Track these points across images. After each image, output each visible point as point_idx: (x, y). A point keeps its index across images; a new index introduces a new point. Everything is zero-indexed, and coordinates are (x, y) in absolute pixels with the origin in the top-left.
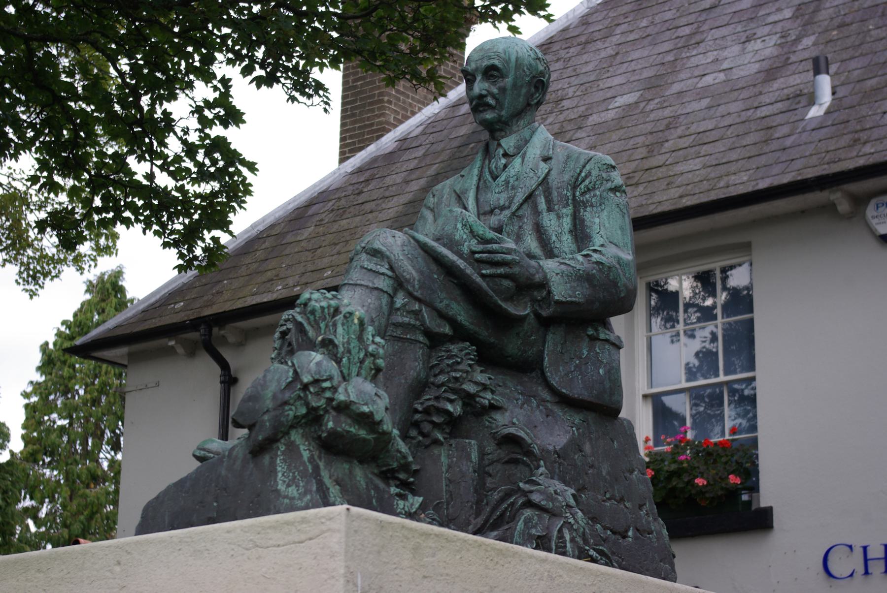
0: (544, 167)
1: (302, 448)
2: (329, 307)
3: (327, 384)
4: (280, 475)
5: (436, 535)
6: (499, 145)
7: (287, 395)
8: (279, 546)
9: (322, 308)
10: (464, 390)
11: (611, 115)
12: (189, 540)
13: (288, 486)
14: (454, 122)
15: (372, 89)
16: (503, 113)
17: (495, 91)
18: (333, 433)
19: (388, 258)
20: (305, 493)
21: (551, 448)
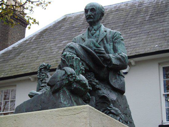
0: (105, 33)
1: (67, 92)
2: (72, 56)
3: (74, 75)
4: (61, 98)
5: (105, 116)
6: (93, 28)
7: (64, 77)
8: (67, 116)
9: (70, 56)
10: (93, 84)
11: (62, 45)
12: (38, 114)
13: (64, 101)
14: (25, 44)
15: (5, 37)
16: (95, 20)
17: (93, 14)
18: (75, 88)
19: (75, 49)
20: (69, 104)
21: (113, 100)
